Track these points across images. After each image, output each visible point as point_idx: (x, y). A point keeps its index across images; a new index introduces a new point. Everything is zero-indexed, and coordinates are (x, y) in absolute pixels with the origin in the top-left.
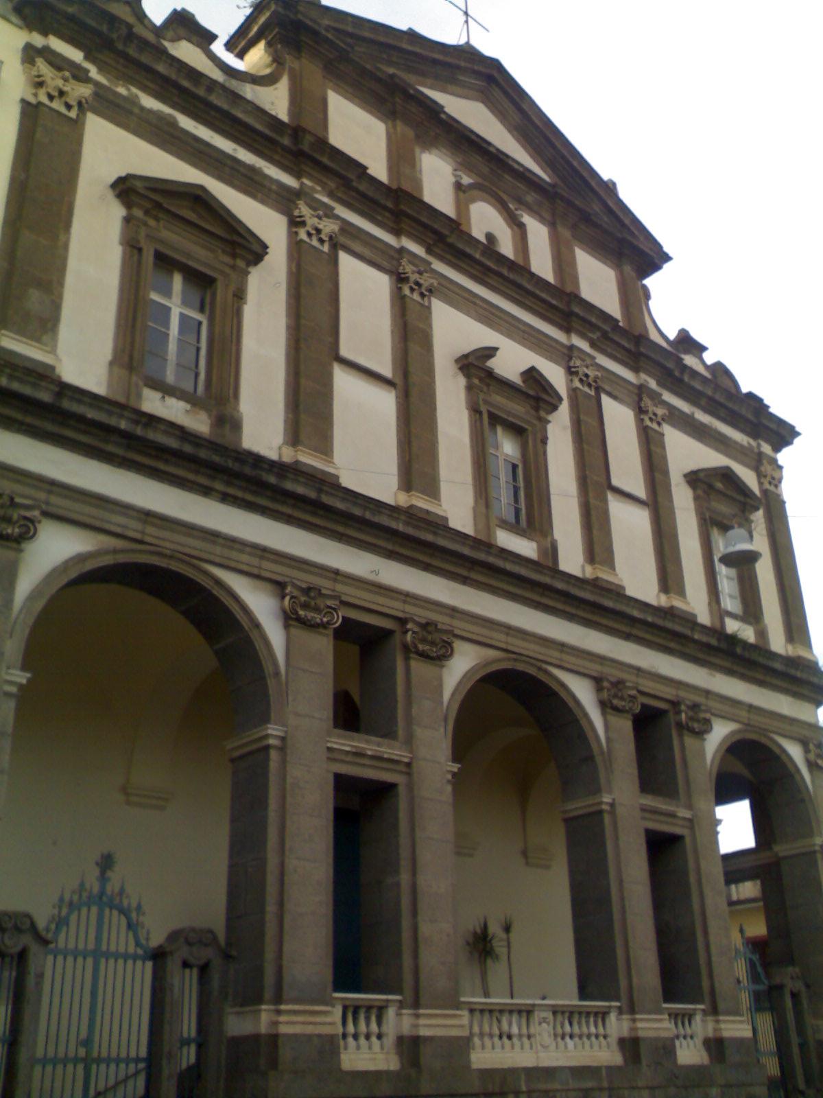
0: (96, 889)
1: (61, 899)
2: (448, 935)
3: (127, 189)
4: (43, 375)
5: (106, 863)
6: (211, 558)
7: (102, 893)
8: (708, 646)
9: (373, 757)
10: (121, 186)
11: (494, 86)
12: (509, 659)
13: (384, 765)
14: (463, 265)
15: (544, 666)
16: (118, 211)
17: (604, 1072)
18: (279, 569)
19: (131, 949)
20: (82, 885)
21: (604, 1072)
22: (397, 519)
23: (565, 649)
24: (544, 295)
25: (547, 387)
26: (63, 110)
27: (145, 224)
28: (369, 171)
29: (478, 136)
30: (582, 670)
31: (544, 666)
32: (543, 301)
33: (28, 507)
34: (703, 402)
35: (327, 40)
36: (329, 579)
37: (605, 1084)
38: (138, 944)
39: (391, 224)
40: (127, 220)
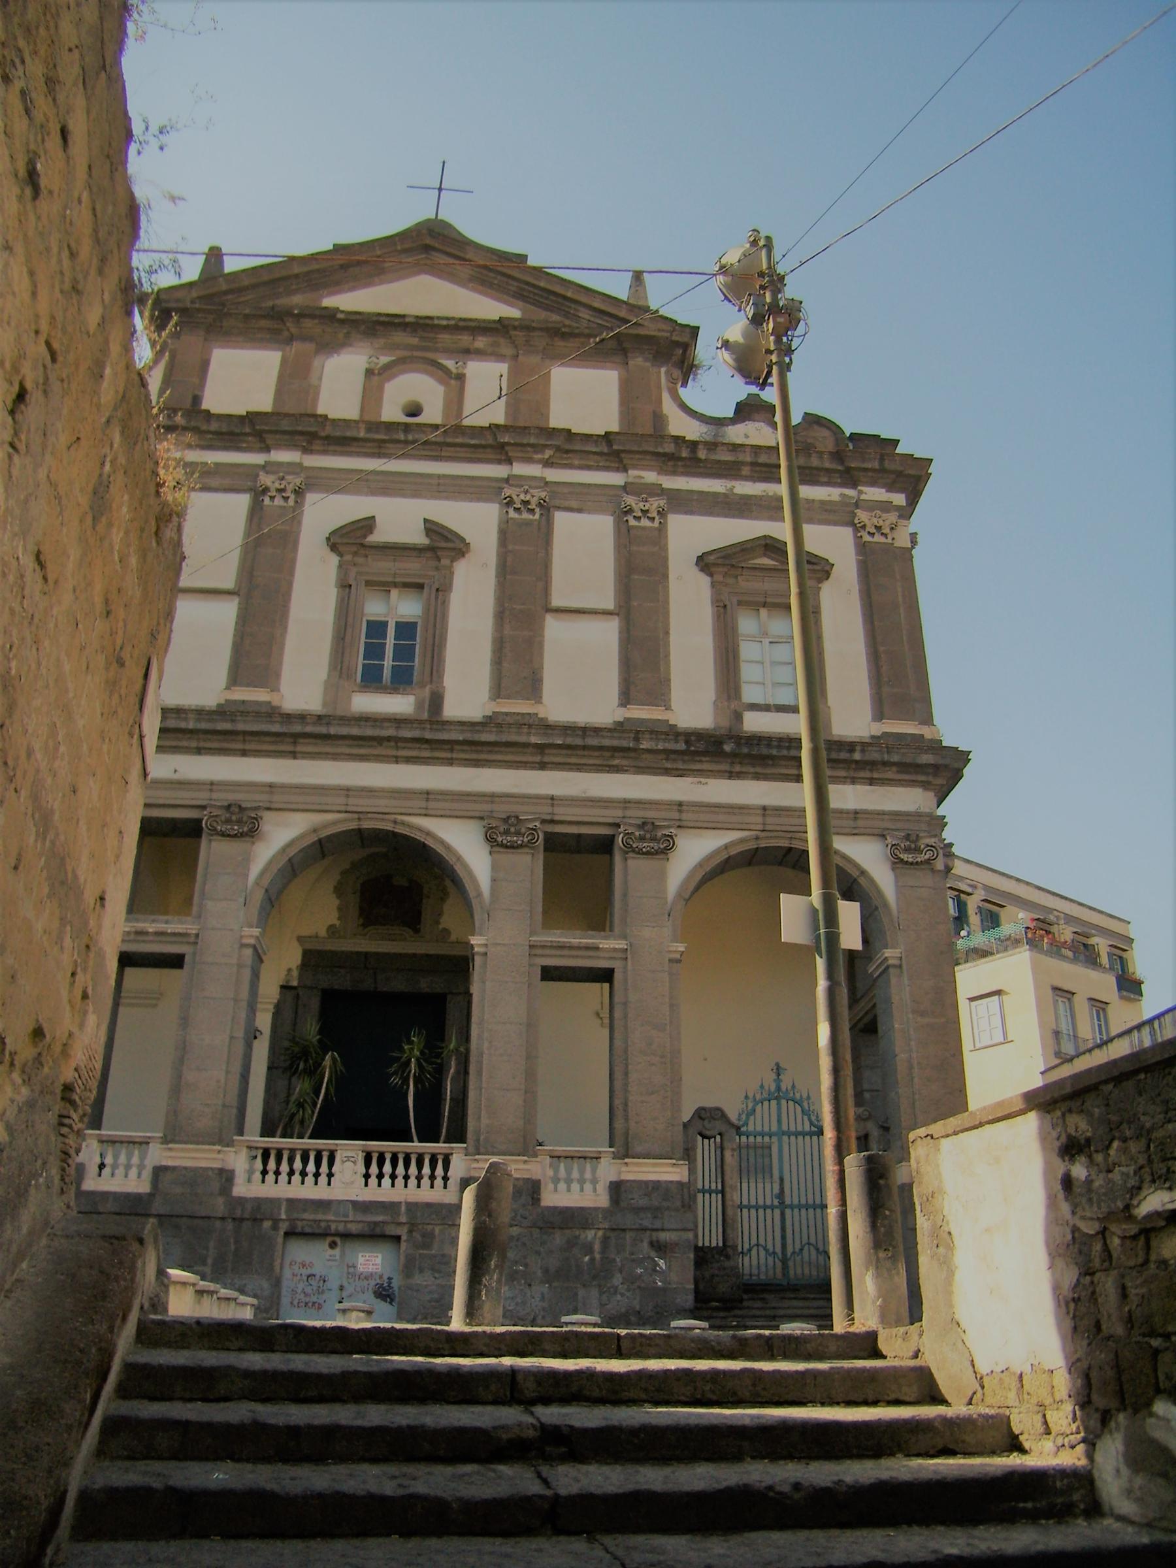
0: (773, 1088)
1: (746, 1097)
2: (218, 1081)
3: (704, 563)
4: (271, 712)
5: (778, 1070)
6: (411, 811)
7: (779, 1089)
8: (668, 753)
9: (157, 934)
10: (702, 564)
11: (433, 253)
12: (352, 820)
13: (169, 939)
14: (353, 449)
15: (399, 817)
16: (704, 581)
17: (403, 1208)
18: (607, 812)
19: (807, 1128)
20: (762, 1086)
21: (403, 1208)
22: (186, 719)
23: (351, 793)
24: (459, 440)
25: (446, 533)
26: (883, 540)
27: (726, 585)
28: (212, 411)
29: (388, 315)
30: (168, 802)
31: (399, 817)
32: (462, 445)
33: (668, 827)
34: (746, 471)
35: (198, 310)
36: (487, 802)
37: (403, 1219)
38: (811, 1124)
39: (258, 445)
40: (713, 585)
